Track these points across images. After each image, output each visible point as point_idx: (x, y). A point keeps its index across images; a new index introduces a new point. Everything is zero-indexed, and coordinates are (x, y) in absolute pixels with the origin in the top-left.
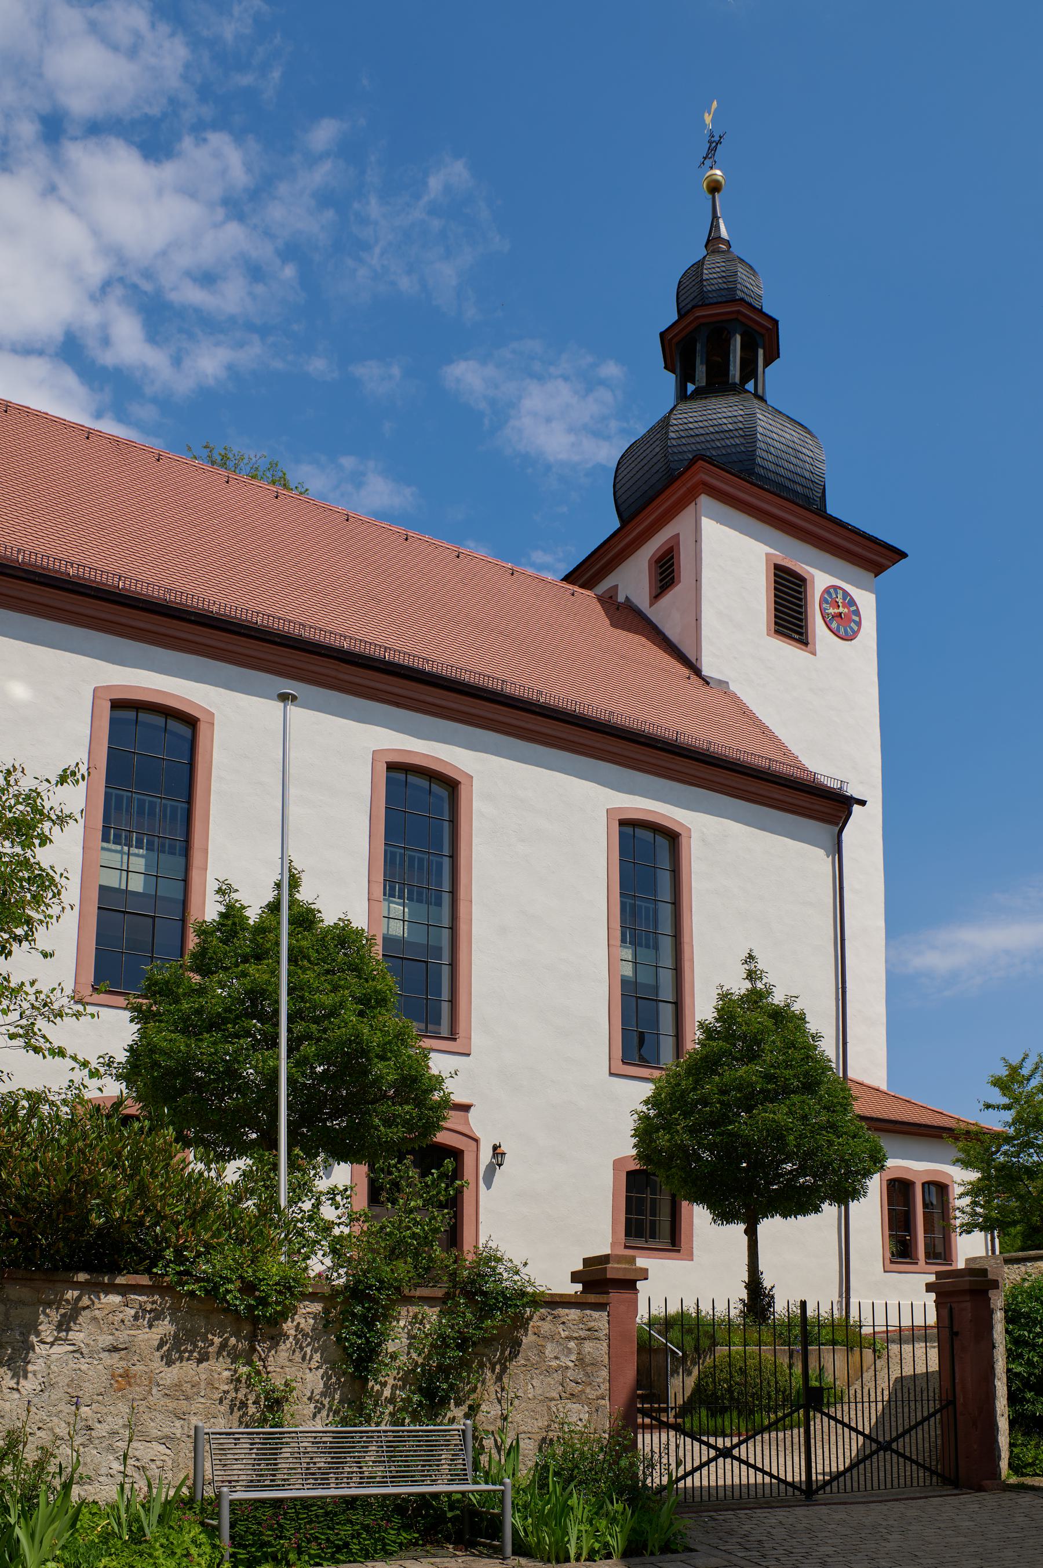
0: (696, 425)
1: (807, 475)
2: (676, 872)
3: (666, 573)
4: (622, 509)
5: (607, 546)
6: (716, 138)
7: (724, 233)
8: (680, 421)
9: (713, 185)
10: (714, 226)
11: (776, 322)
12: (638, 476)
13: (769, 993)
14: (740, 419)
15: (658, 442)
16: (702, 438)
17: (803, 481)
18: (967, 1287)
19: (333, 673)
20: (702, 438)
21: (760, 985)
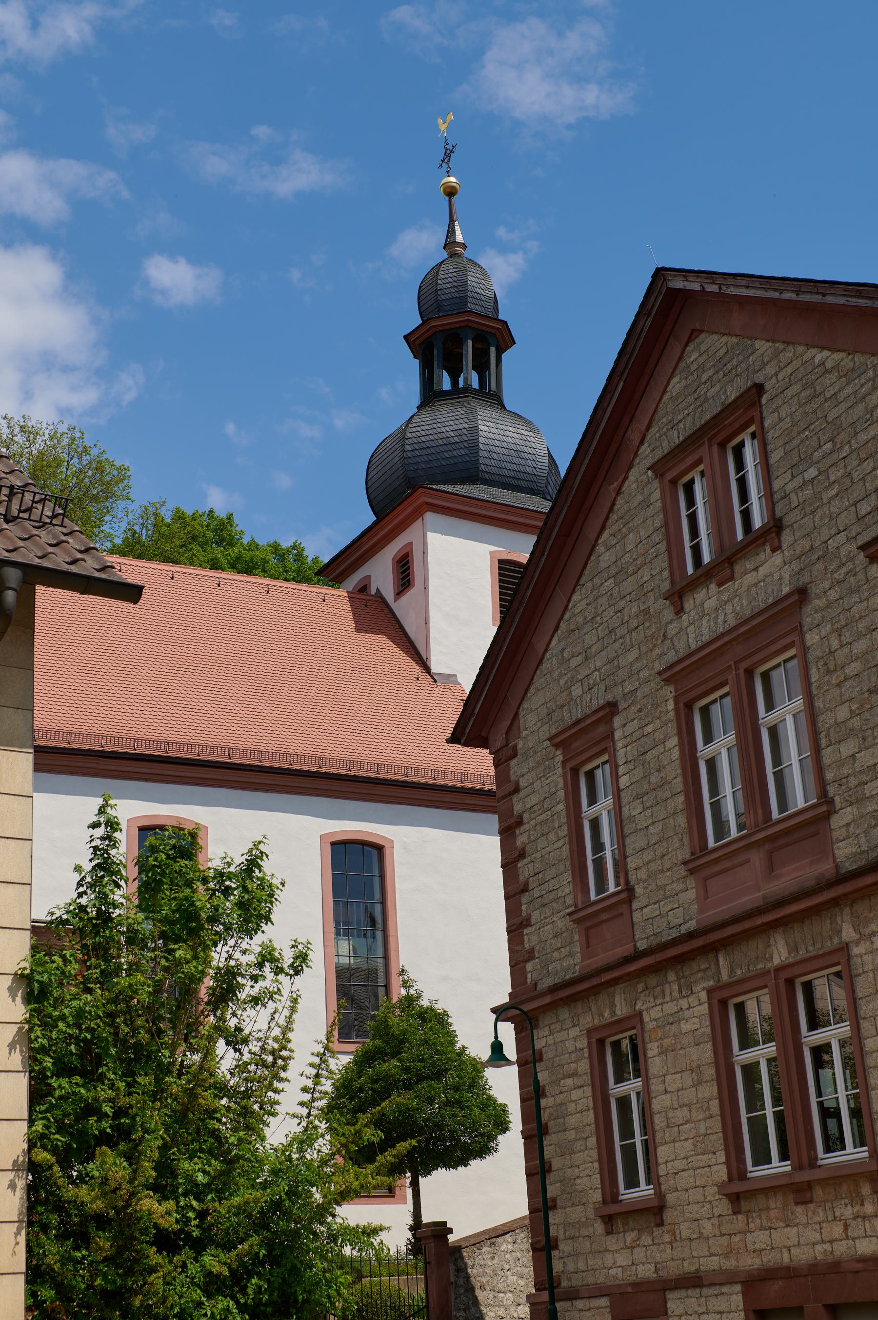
0: (427, 438)
1: (529, 470)
2: (382, 877)
3: (405, 573)
4: (374, 504)
5: (359, 543)
6: (449, 147)
7: (459, 238)
8: (414, 434)
9: (448, 190)
10: (451, 231)
11: (506, 322)
12: (384, 479)
13: (419, 997)
14: (465, 432)
15: (396, 453)
16: (433, 450)
17: (527, 477)
18: (430, 1234)
19: (95, 766)
20: (433, 450)
21: (412, 992)
